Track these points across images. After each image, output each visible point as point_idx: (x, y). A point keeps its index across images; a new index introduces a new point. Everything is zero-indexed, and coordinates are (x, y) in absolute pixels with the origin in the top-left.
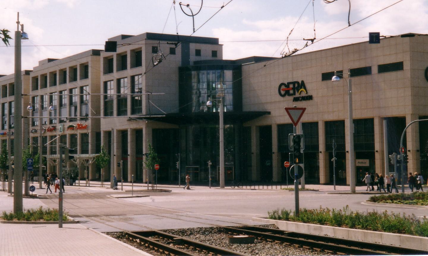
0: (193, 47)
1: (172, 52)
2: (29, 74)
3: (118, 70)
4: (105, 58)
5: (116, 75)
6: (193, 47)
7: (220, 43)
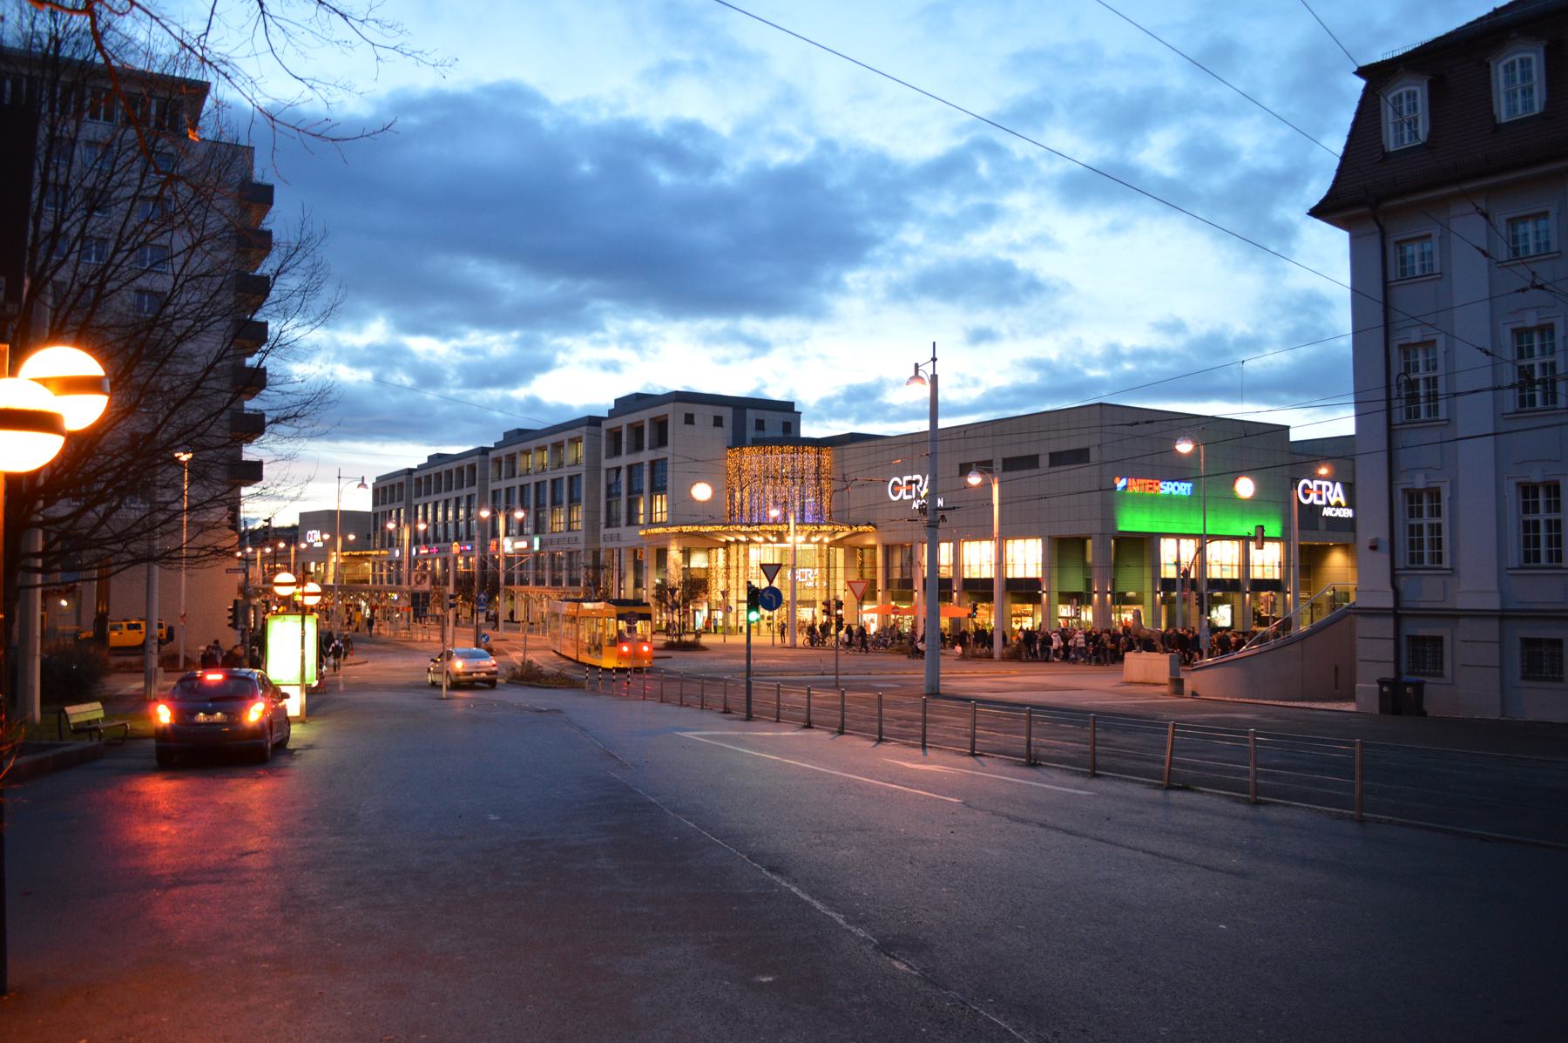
0: (752, 415)
1: (718, 422)
2: (600, 425)
3: (628, 453)
4: (609, 431)
5: (624, 460)
6: (752, 415)
7: (796, 410)
